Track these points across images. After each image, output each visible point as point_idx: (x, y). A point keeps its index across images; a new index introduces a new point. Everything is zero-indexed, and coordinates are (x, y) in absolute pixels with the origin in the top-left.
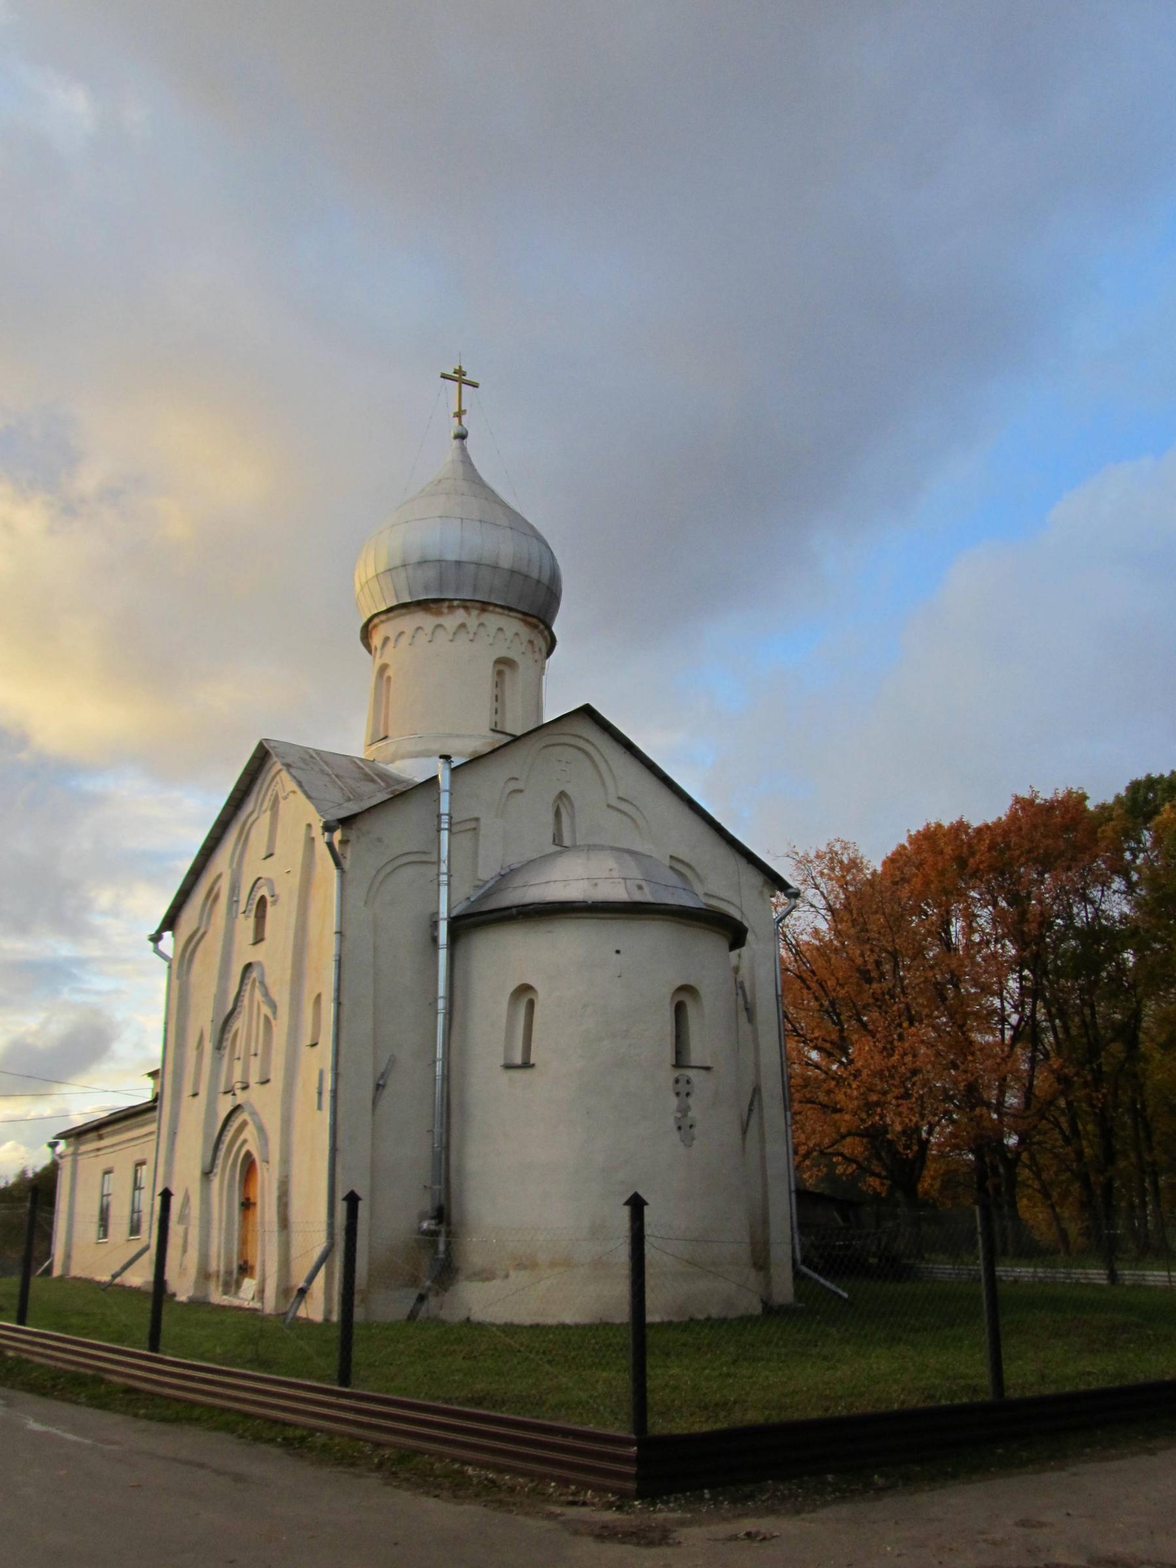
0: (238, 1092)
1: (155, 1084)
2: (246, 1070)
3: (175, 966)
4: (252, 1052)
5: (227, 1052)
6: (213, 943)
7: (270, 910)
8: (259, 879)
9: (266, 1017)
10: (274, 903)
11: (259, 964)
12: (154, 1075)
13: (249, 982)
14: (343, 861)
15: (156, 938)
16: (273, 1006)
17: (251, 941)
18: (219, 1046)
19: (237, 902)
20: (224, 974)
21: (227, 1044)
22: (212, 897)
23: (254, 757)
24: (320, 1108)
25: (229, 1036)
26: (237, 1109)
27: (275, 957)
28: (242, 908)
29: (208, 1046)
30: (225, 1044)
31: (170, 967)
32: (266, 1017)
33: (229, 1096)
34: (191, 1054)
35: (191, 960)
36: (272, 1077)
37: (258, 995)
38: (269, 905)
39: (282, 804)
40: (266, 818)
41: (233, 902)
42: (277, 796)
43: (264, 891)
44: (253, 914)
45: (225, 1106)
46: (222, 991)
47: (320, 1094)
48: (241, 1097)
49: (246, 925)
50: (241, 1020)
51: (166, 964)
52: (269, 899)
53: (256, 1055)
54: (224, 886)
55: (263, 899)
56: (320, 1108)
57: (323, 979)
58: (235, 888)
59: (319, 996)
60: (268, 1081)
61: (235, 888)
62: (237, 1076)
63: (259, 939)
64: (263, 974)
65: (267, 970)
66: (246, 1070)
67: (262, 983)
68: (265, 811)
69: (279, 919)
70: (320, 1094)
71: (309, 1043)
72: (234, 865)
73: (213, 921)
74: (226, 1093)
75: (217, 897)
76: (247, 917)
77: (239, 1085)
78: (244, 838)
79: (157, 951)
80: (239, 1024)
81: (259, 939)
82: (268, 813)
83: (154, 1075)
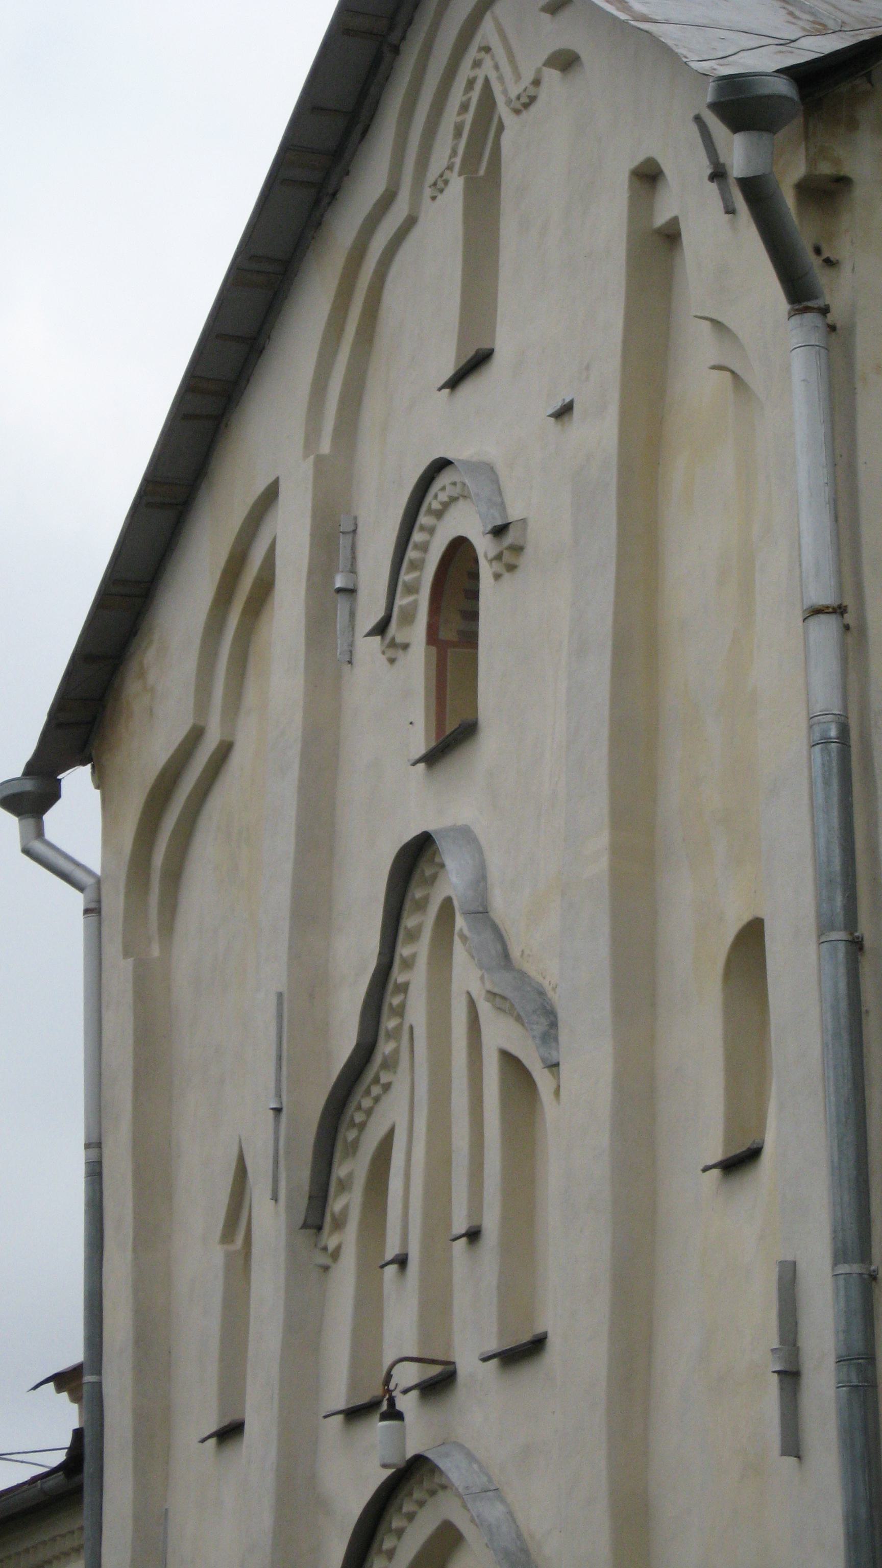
0: (407, 1403)
1: (80, 1408)
2: (436, 1308)
3: (115, 904)
4: (460, 1225)
5: (348, 1239)
6: (259, 795)
7: (491, 593)
8: (441, 465)
9: (511, 1062)
10: (511, 558)
11: (465, 834)
12: (66, 1381)
13: (421, 921)
14: (821, 277)
15: (32, 798)
16: (547, 1021)
17: (420, 745)
18: (315, 1216)
19: (350, 592)
20: (312, 909)
21: (348, 1202)
22: (245, 592)
23: (405, 221)
24: (793, 1445)
25: (353, 1169)
26: (410, 1477)
27: (527, 820)
28: (370, 609)
29: (270, 1221)
30: (336, 1205)
31: (93, 911)
32: (511, 1062)
33: (378, 1429)
34: (198, 1257)
35: (174, 875)
36: (551, 1321)
37: (467, 975)
38: (486, 571)
39: (514, 132)
40: (443, 222)
41: (332, 595)
42: (488, 101)
43: (467, 522)
44: (417, 633)
45: (353, 1473)
46: (308, 983)
47: (790, 1377)
48: (418, 1431)
49: (391, 693)
50: (400, 1081)
51: (76, 900)
52: (483, 546)
53: (473, 1235)
54: (291, 535)
55: (459, 548)
56: (793, 1445)
57: (761, 857)
58: (334, 536)
59: (752, 936)
60: (535, 1346)
61: (334, 536)
62: (401, 1332)
63: (452, 739)
64: (481, 879)
65: (495, 862)
66: (436, 1308)
67: (481, 913)
68: (441, 185)
69: (540, 638)
70: (790, 1377)
71: (717, 1154)
72: (325, 447)
73: (251, 697)
74: (355, 1414)
75: (265, 587)
76: (396, 649)
77: (408, 1375)
78: (362, 321)
79: (39, 852)
80: (398, 1109)
81: (452, 739)
82: (457, 184)
83: (66, 1381)
